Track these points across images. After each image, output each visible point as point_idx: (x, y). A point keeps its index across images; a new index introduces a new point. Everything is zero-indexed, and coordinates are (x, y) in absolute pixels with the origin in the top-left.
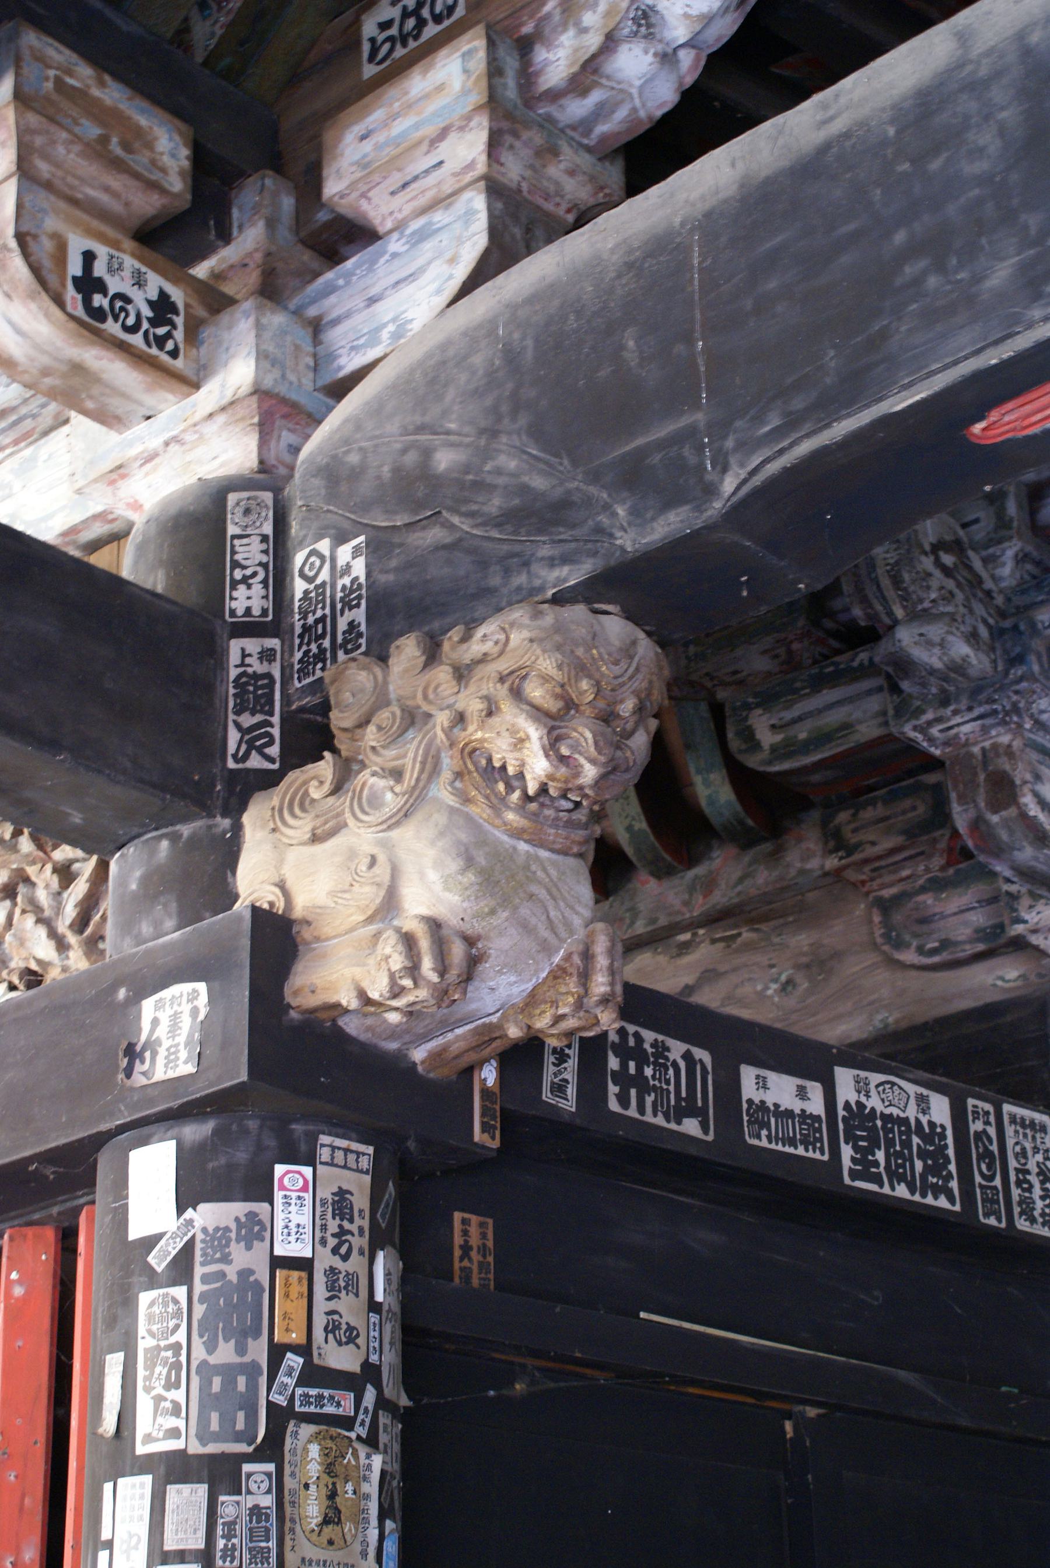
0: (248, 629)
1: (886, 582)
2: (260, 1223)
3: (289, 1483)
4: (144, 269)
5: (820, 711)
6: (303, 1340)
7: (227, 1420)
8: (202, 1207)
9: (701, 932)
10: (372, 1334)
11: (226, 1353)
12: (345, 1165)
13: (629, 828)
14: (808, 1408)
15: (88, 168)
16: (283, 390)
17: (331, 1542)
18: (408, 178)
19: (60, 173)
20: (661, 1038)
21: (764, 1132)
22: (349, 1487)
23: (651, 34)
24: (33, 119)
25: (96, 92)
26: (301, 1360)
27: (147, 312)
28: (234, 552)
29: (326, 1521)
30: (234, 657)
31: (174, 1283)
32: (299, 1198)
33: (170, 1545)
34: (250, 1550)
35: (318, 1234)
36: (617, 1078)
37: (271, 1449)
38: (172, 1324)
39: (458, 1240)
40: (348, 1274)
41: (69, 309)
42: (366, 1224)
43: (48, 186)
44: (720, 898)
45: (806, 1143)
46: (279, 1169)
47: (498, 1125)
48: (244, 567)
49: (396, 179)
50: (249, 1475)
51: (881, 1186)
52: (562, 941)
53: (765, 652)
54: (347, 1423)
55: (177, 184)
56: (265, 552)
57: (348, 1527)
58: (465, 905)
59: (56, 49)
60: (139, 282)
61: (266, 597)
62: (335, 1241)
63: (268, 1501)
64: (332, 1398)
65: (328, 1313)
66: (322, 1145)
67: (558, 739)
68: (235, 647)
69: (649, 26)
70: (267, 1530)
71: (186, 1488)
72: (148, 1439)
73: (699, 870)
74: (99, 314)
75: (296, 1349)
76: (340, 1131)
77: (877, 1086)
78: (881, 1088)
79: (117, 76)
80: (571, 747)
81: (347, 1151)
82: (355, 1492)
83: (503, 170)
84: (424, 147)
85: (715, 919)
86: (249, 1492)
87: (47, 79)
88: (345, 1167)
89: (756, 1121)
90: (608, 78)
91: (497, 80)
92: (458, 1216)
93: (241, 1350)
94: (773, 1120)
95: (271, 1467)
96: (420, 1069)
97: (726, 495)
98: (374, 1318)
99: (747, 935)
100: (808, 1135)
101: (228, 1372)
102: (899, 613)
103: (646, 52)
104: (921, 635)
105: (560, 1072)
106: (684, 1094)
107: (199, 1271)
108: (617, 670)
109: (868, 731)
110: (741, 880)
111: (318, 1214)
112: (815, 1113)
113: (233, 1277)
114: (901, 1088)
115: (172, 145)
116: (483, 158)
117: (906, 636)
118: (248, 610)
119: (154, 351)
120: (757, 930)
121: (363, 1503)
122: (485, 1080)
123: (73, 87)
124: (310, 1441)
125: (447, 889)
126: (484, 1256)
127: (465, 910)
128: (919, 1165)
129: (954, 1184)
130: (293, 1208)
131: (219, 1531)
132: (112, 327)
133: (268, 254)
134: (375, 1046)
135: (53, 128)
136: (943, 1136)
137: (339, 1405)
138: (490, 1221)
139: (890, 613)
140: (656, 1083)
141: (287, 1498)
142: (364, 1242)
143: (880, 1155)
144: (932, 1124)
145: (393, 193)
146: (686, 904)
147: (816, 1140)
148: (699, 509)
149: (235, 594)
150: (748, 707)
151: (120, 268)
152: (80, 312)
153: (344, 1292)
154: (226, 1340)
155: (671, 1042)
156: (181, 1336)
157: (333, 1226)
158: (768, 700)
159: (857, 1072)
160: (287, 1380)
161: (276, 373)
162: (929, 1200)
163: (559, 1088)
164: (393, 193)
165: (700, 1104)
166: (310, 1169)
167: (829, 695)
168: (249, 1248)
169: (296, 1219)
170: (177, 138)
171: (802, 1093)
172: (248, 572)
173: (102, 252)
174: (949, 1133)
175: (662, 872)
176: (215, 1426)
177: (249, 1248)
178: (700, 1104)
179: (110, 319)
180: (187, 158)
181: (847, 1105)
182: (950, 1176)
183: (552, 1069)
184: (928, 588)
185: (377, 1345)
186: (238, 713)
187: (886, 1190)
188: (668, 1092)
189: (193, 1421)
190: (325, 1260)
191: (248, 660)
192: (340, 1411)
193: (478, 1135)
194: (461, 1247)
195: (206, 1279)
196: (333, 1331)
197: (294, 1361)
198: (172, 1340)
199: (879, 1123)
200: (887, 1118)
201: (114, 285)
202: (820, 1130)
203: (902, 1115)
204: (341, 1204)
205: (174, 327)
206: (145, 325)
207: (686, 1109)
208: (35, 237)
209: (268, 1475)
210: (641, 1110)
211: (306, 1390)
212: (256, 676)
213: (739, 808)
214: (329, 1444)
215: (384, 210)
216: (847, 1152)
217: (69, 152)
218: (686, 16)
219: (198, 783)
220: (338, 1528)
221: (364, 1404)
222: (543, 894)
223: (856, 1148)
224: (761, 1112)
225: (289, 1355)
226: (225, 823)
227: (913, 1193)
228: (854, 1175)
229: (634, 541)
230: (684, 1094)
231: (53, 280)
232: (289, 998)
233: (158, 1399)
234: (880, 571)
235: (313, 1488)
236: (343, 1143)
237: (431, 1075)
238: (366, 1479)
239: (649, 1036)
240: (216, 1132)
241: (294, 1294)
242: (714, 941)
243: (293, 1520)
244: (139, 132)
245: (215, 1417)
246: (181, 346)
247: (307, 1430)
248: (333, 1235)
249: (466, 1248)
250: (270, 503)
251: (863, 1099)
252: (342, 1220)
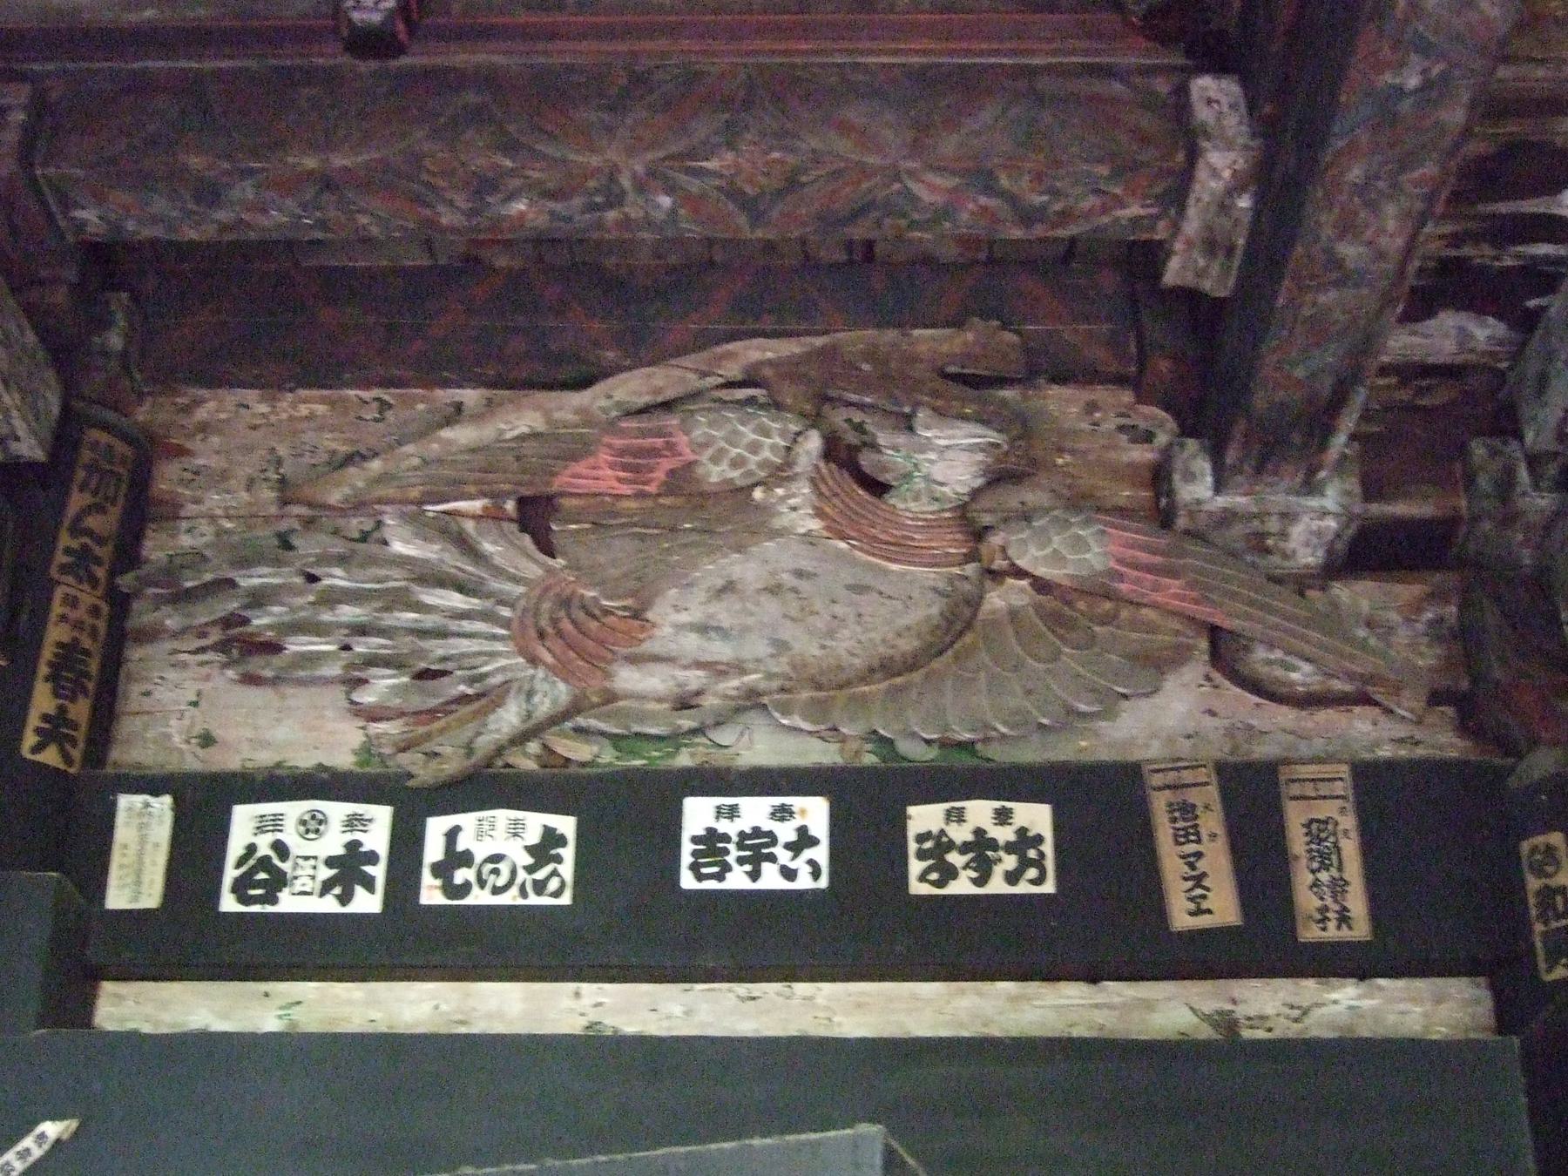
60: (516, 831)
205: (558, 859)
206: (522, 875)
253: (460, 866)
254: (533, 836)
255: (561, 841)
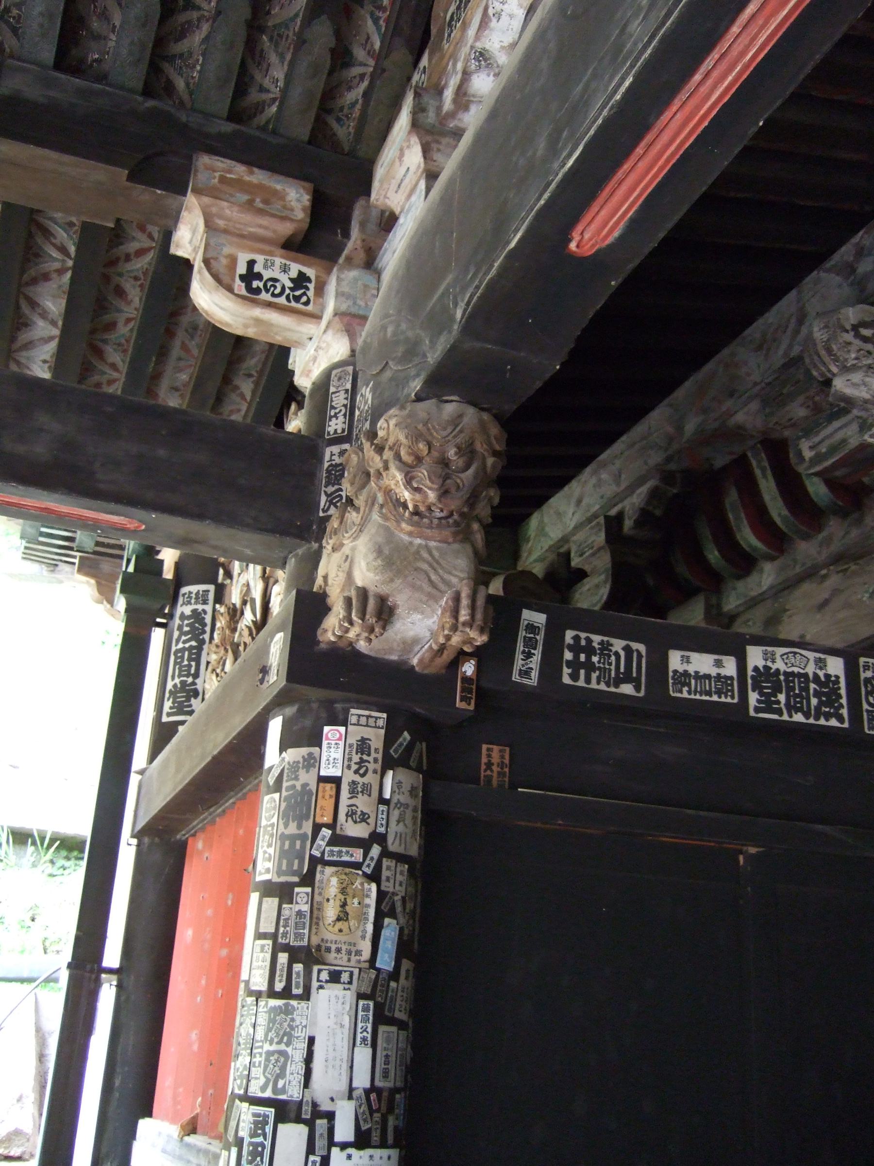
0: (337, 440)
1: (823, 353)
2: (314, 758)
3: (317, 898)
4: (288, 263)
5: (832, 435)
6: (330, 821)
7: (290, 864)
8: (290, 751)
9: (832, 568)
10: (380, 816)
11: (292, 829)
12: (367, 725)
13: (779, 515)
14: (750, 848)
15: (247, 217)
16: (354, 310)
17: (340, 931)
18: (399, 181)
19: (231, 224)
20: (606, 639)
21: (685, 689)
22: (356, 901)
23: (489, 64)
24: (206, 200)
25: (247, 178)
26: (330, 832)
27: (289, 284)
28: (332, 401)
29: (339, 919)
30: (327, 457)
31: (276, 792)
32: (336, 744)
33: (261, 930)
34: (295, 934)
35: (346, 763)
36: (569, 664)
37: (308, 880)
38: (272, 813)
39: (484, 760)
40: (364, 784)
41: (236, 292)
42: (380, 756)
43: (226, 231)
44: (835, 547)
45: (719, 693)
46: (326, 729)
47: (474, 697)
48: (336, 408)
49: (394, 184)
50: (298, 894)
51: (781, 714)
52: (196, 603)
53: (801, 405)
54: (357, 866)
55: (300, 215)
56: (346, 399)
57: (353, 923)
58: (377, 578)
59: (222, 162)
60: (285, 269)
61: (345, 423)
62: (357, 767)
63: (306, 908)
64: (348, 852)
65: (348, 806)
66: (352, 715)
67: (412, 478)
68: (328, 451)
69: (485, 60)
70: (304, 923)
71: (270, 900)
72: (260, 874)
73: (824, 534)
74: (258, 291)
75: (327, 826)
76: (365, 706)
77: (782, 656)
78: (785, 657)
79: (260, 167)
80: (417, 482)
81: (368, 717)
82: (359, 903)
83: (435, 164)
84: (397, 163)
85: (838, 559)
86: (297, 903)
87: (214, 178)
88: (367, 726)
89: (680, 682)
90: (473, 96)
91: (421, 116)
92: (484, 747)
93: (299, 827)
94: (693, 682)
95: (309, 890)
96: (417, 669)
97: (458, 320)
98: (382, 807)
99: (853, 567)
100: (722, 688)
101: (293, 838)
102: (835, 370)
103: (488, 75)
104: (848, 380)
105: (527, 664)
106: (622, 670)
107: (285, 784)
108: (445, 433)
109: (854, 443)
110: (843, 537)
111: (347, 752)
112: (728, 675)
113: (299, 788)
114: (801, 655)
115: (298, 195)
116: (422, 160)
117: (840, 384)
118: (336, 430)
119: (293, 304)
120: (858, 564)
121: (365, 909)
122: (465, 672)
123: (231, 179)
124: (332, 876)
125: (368, 570)
126: (502, 768)
127: (377, 581)
128: (814, 701)
129: (844, 712)
130: (332, 750)
131: (281, 923)
132: (265, 296)
133: (363, 241)
134: (384, 659)
135: (218, 201)
136: (837, 681)
137: (352, 856)
138: (508, 749)
139: (829, 371)
140: (601, 665)
141: (315, 904)
142: (378, 767)
143: (782, 697)
144: (828, 676)
145: (396, 192)
146: (819, 553)
147: (728, 691)
148: (450, 332)
149: (331, 423)
150: (799, 438)
151: (273, 264)
152: (244, 292)
153: (360, 794)
154: (293, 821)
155: (613, 641)
156: (275, 820)
157: (356, 758)
158: (808, 432)
159: (764, 648)
160: (321, 843)
161: (350, 302)
162: (822, 722)
163: (526, 673)
164: (396, 192)
165: (634, 675)
166: (344, 728)
167: (836, 424)
168: (308, 772)
169: (333, 755)
170: (302, 191)
171: (718, 664)
172: (337, 411)
173: (260, 259)
174: (842, 681)
175: (806, 537)
176: (284, 867)
177: (308, 772)
178: (634, 675)
179: (263, 292)
180: (308, 200)
181: (756, 669)
182: (841, 706)
183: (521, 662)
184: (849, 351)
185: (384, 822)
186: (326, 487)
187: (785, 717)
188: (610, 670)
189: (276, 864)
190: (349, 777)
191: (333, 458)
192: (353, 859)
193: (459, 704)
194: (485, 764)
195: (287, 789)
196: (351, 816)
197: (326, 833)
198: (271, 822)
199: (782, 678)
200: (786, 674)
201: (267, 274)
202: (732, 685)
203: (802, 671)
204: (363, 746)
205: (308, 289)
206: (287, 291)
207: (627, 678)
208: (216, 259)
209: (307, 894)
210: (588, 680)
211: (332, 848)
212: (337, 465)
213: (832, 496)
214: (344, 877)
215: (396, 202)
216: (753, 698)
217: (232, 212)
218: (502, 48)
219: (299, 526)
220: (346, 924)
221: (370, 855)
222: (425, 566)
223: (761, 694)
224: (683, 678)
225: (324, 829)
226: (315, 546)
227: (807, 718)
228: (757, 710)
229: (432, 358)
230: (622, 670)
231: (226, 279)
232: (320, 638)
233: (265, 852)
234: (820, 347)
235: (332, 901)
236: (367, 713)
237: (426, 672)
238: (368, 896)
239: (596, 639)
240: (299, 711)
241: (327, 797)
242: (838, 572)
243: (318, 918)
244: (275, 193)
245: (285, 862)
246: (312, 299)
247: (329, 870)
248: (356, 763)
249: (489, 765)
250: (351, 372)
251: (769, 664)
252: (362, 754)
253: (256, 280)
254: (294, 274)
255: (309, 280)
